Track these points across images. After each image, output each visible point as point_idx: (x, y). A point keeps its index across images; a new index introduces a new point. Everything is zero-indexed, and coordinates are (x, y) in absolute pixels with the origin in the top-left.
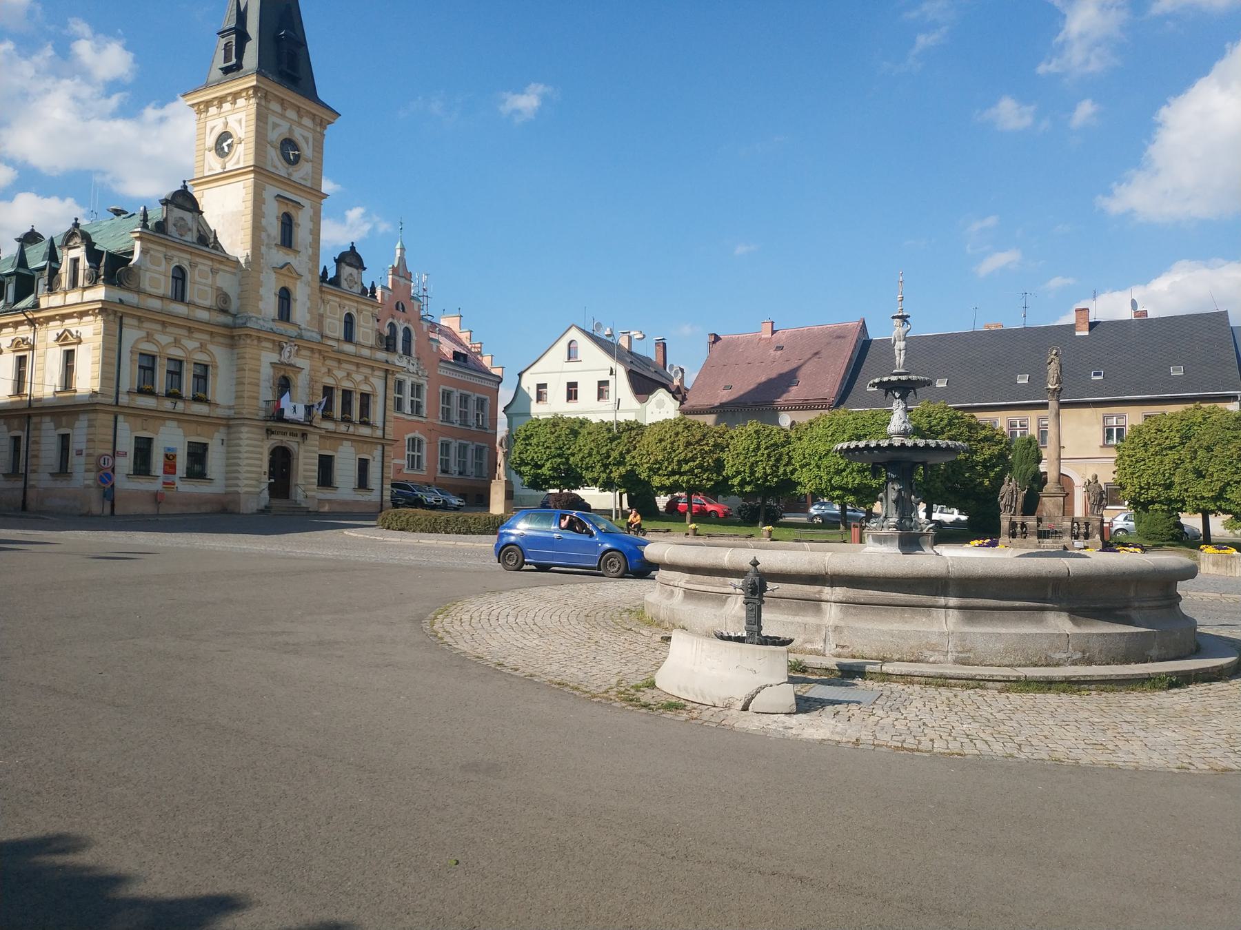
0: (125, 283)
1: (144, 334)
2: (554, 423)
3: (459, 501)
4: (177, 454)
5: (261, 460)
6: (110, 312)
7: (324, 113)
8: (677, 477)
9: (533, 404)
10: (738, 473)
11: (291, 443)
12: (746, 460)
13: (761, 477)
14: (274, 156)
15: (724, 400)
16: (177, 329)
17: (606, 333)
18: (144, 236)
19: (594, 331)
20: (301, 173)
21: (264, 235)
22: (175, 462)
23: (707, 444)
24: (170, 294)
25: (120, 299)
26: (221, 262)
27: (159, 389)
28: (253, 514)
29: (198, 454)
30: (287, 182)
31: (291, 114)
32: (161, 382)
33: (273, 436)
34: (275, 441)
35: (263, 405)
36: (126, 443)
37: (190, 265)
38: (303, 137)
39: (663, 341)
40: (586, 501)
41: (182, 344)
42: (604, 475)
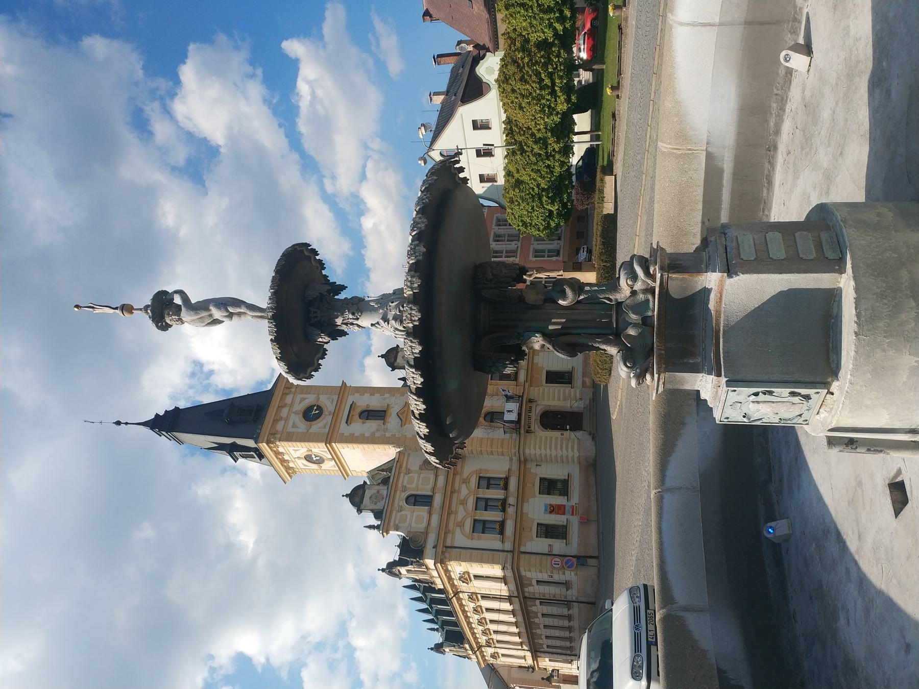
0: (421, 544)
1: (458, 530)
6: (443, 557)
7: (267, 427)
8: (556, 88)
10: (550, 25)
11: (537, 410)
12: (537, 17)
14: (317, 426)
16: (450, 522)
17: (423, 165)
19: (431, 131)
20: (328, 404)
21: (378, 434)
22: (556, 505)
23: (522, 59)
25: (433, 548)
26: (401, 466)
27: (500, 495)
28: (596, 445)
29: (549, 486)
30: (336, 414)
31: (284, 412)
32: (494, 516)
33: (532, 428)
34: (535, 425)
35: (508, 435)
36: (541, 545)
37: (405, 491)
39: (436, 57)
42: (557, 157)
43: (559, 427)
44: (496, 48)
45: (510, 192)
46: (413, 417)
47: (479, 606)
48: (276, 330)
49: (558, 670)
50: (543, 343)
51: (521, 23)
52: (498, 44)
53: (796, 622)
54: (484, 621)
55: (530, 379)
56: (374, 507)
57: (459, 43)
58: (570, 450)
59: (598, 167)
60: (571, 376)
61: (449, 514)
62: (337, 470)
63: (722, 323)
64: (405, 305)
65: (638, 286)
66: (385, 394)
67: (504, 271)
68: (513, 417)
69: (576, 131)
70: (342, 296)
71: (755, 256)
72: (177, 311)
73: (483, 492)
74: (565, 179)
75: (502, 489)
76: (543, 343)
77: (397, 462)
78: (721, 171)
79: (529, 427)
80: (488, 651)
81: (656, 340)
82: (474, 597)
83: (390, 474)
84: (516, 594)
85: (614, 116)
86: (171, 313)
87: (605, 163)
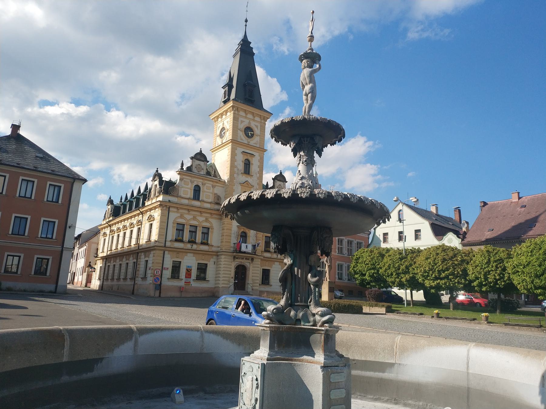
0: (172, 193)
1: (179, 215)
2: (371, 250)
3: (340, 294)
4: (192, 269)
5: (230, 271)
6: (164, 206)
8: (439, 281)
9: (382, 243)
10: (477, 278)
11: (246, 263)
12: (482, 270)
13: (493, 281)
14: (241, 135)
15: (488, 237)
16: (195, 212)
17: (394, 199)
18: (181, 173)
19: (415, 205)
20: (254, 141)
21: (236, 169)
23: (457, 260)
24: (192, 197)
25: (169, 200)
26: (217, 182)
29: (202, 269)
30: (248, 145)
31: (250, 116)
32: (186, 236)
33: (236, 260)
34: (238, 262)
35: (233, 245)
36: (168, 264)
38: (255, 125)
40: (399, 295)
41: (197, 219)
42: (397, 280)
43: (237, 276)
44: (464, 245)
45: (377, 251)
46: (249, 192)
47: (134, 226)
48: (298, 120)
49: (95, 271)
50: (287, 264)
51: (478, 259)
52: (466, 246)
53: (127, 404)
54: (125, 229)
55: (265, 259)
56: (194, 167)
57: (467, 223)
58: (223, 282)
59: (391, 304)
60: (266, 284)
61: (188, 210)
62: (216, 146)
63: (296, 363)
64: (309, 189)
65: (317, 318)
66: (259, 174)
67: (327, 244)
68: (243, 248)
69: (413, 292)
70: (315, 154)
71: (332, 382)
72: (309, 66)
73: (200, 230)
74: (384, 285)
75: (201, 241)
76: (287, 264)
77: (220, 180)
78: (384, 372)
79: (237, 258)
80: (107, 231)
81: (288, 326)
82: (140, 224)
83: (212, 176)
84: (140, 248)
85: (421, 314)
86: (308, 63)
87: (393, 308)
